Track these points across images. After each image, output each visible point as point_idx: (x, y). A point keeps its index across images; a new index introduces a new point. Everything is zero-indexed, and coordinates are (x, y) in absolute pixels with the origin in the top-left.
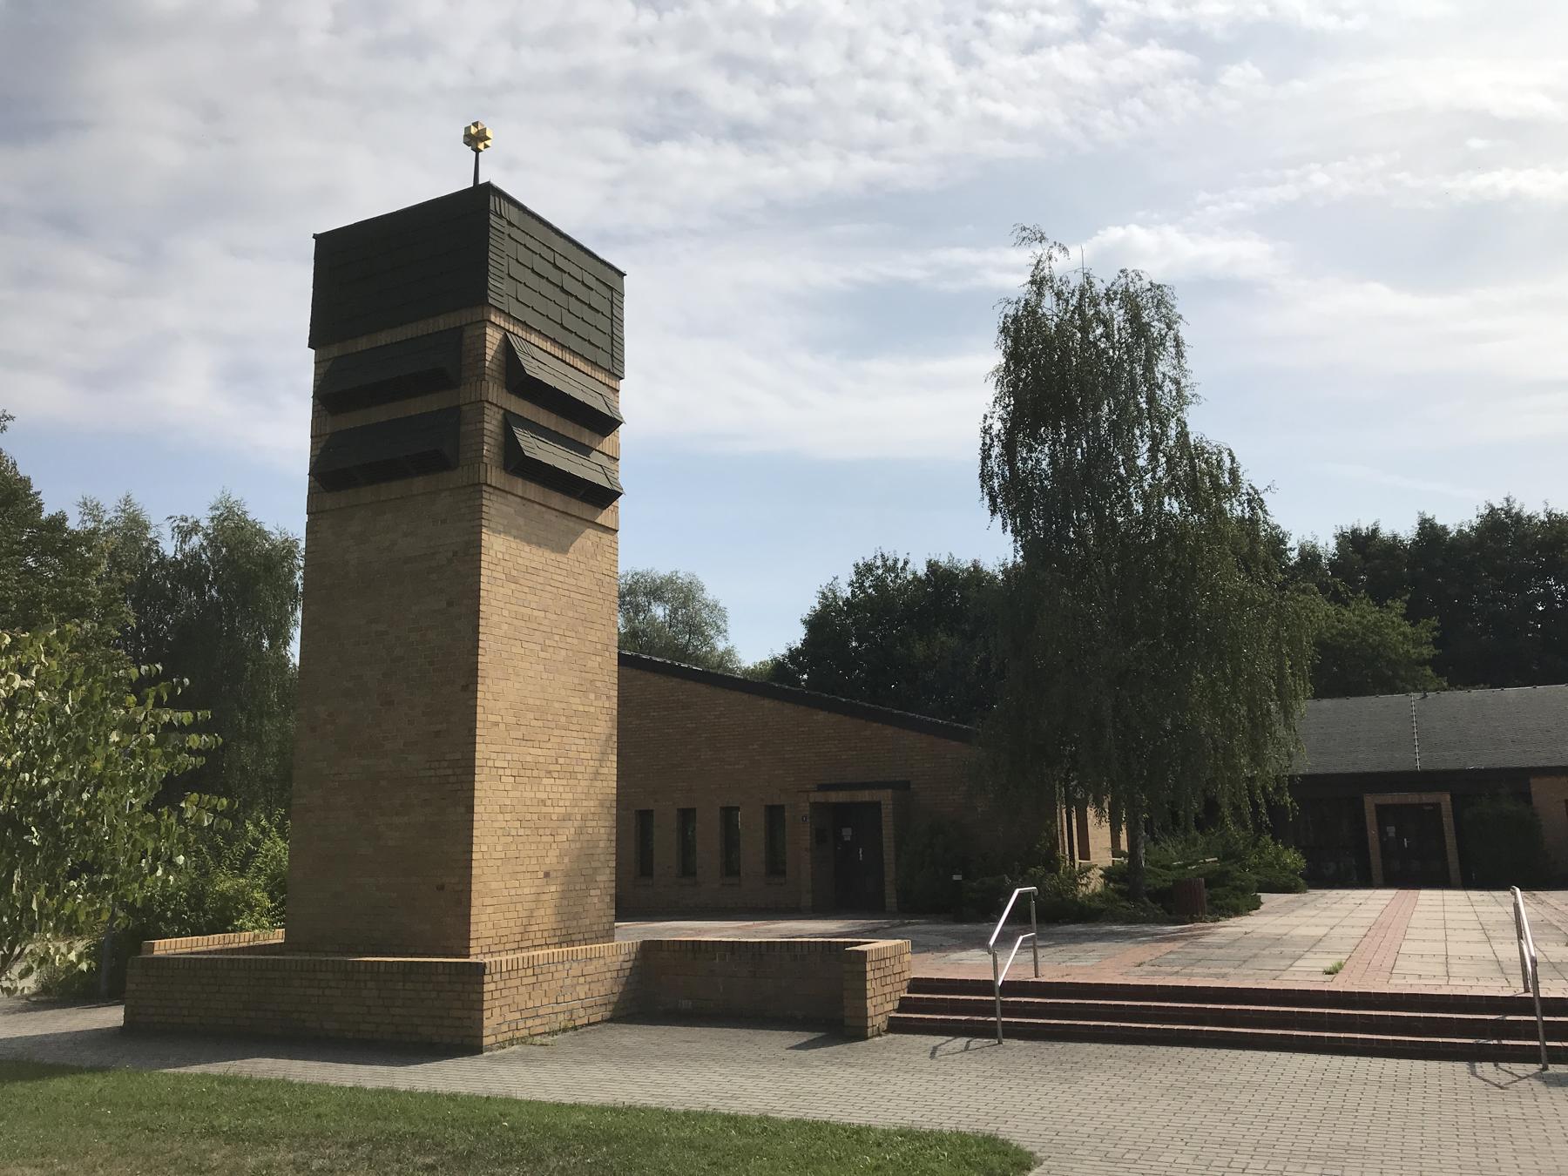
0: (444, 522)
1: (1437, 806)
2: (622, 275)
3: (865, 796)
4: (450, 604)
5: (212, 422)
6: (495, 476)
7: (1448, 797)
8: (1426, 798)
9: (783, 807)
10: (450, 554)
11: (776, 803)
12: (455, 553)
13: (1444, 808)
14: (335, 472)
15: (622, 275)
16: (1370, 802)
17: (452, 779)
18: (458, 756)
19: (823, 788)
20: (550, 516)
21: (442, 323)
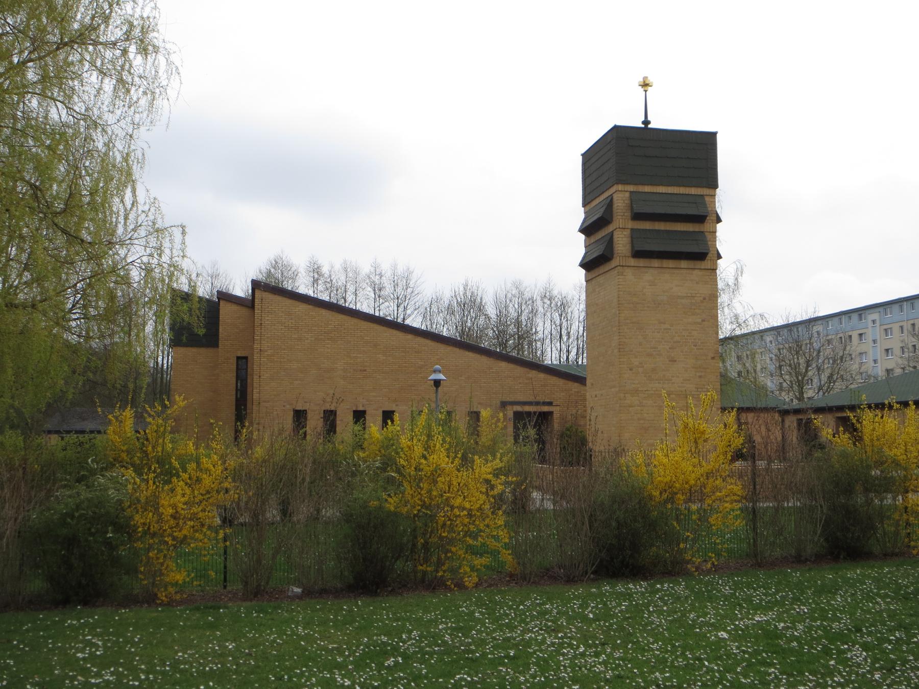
0: (697, 283)
4: (703, 321)
12: (704, 299)
21: (693, 191)
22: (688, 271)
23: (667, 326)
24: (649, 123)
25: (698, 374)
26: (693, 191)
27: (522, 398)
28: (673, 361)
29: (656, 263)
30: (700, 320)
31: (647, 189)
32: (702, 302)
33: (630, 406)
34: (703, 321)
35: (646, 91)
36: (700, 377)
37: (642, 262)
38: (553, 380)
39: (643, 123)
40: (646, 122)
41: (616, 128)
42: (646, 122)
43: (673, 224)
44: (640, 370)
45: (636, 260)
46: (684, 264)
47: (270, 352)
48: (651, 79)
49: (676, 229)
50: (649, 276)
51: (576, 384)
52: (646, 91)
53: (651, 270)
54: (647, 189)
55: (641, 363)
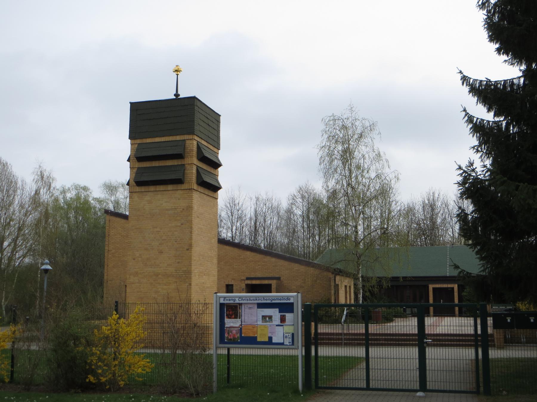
0: (179, 199)
1: (453, 288)
2: (220, 116)
3: (266, 282)
4: (182, 224)
5: (95, 162)
6: (195, 186)
7: (457, 285)
8: (450, 286)
9: (232, 285)
10: (181, 210)
11: (230, 283)
12: (183, 209)
13: (273, 287)
14: (141, 181)
15: (220, 116)
16: (431, 287)
17: (184, 276)
18: (186, 269)
19: (248, 279)
20: (205, 196)
21: (178, 138)
22: (173, 192)
23: (158, 229)
24: (179, 95)
25: (177, 261)
26: (178, 138)
27: (259, 275)
28: (161, 252)
29: (152, 188)
30: (180, 224)
31: (149, 140)
32: (182, 212)
33: (133, 283)
34: (182, 224)
35: (177, 75)
36: (178, 263)
37: (143, 189)
38: (281, 262)
39: (175, 95)
40: (177, 95)
41: (194, 98)
42: (177, 95)
43: (164, 161)
44: (140, 259)
45: (140, 187)
46: (170, 187)
47: (113, 251)
48: (181, 67)
49: (166, 164)
50: (148, 197)
51: (297, 265)
52: (177, 75)
53: (150, 194)
54: (149, 140)
55: (140, 255)
